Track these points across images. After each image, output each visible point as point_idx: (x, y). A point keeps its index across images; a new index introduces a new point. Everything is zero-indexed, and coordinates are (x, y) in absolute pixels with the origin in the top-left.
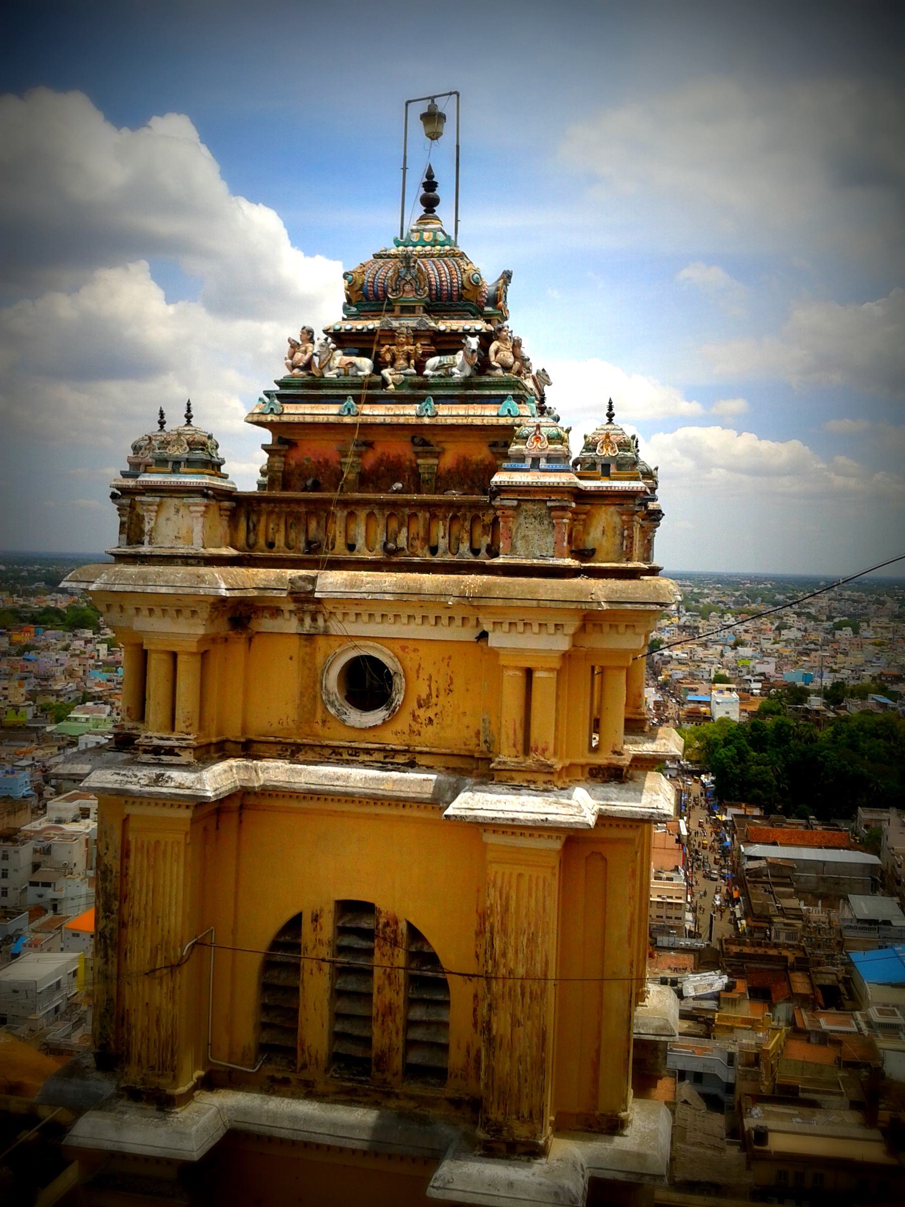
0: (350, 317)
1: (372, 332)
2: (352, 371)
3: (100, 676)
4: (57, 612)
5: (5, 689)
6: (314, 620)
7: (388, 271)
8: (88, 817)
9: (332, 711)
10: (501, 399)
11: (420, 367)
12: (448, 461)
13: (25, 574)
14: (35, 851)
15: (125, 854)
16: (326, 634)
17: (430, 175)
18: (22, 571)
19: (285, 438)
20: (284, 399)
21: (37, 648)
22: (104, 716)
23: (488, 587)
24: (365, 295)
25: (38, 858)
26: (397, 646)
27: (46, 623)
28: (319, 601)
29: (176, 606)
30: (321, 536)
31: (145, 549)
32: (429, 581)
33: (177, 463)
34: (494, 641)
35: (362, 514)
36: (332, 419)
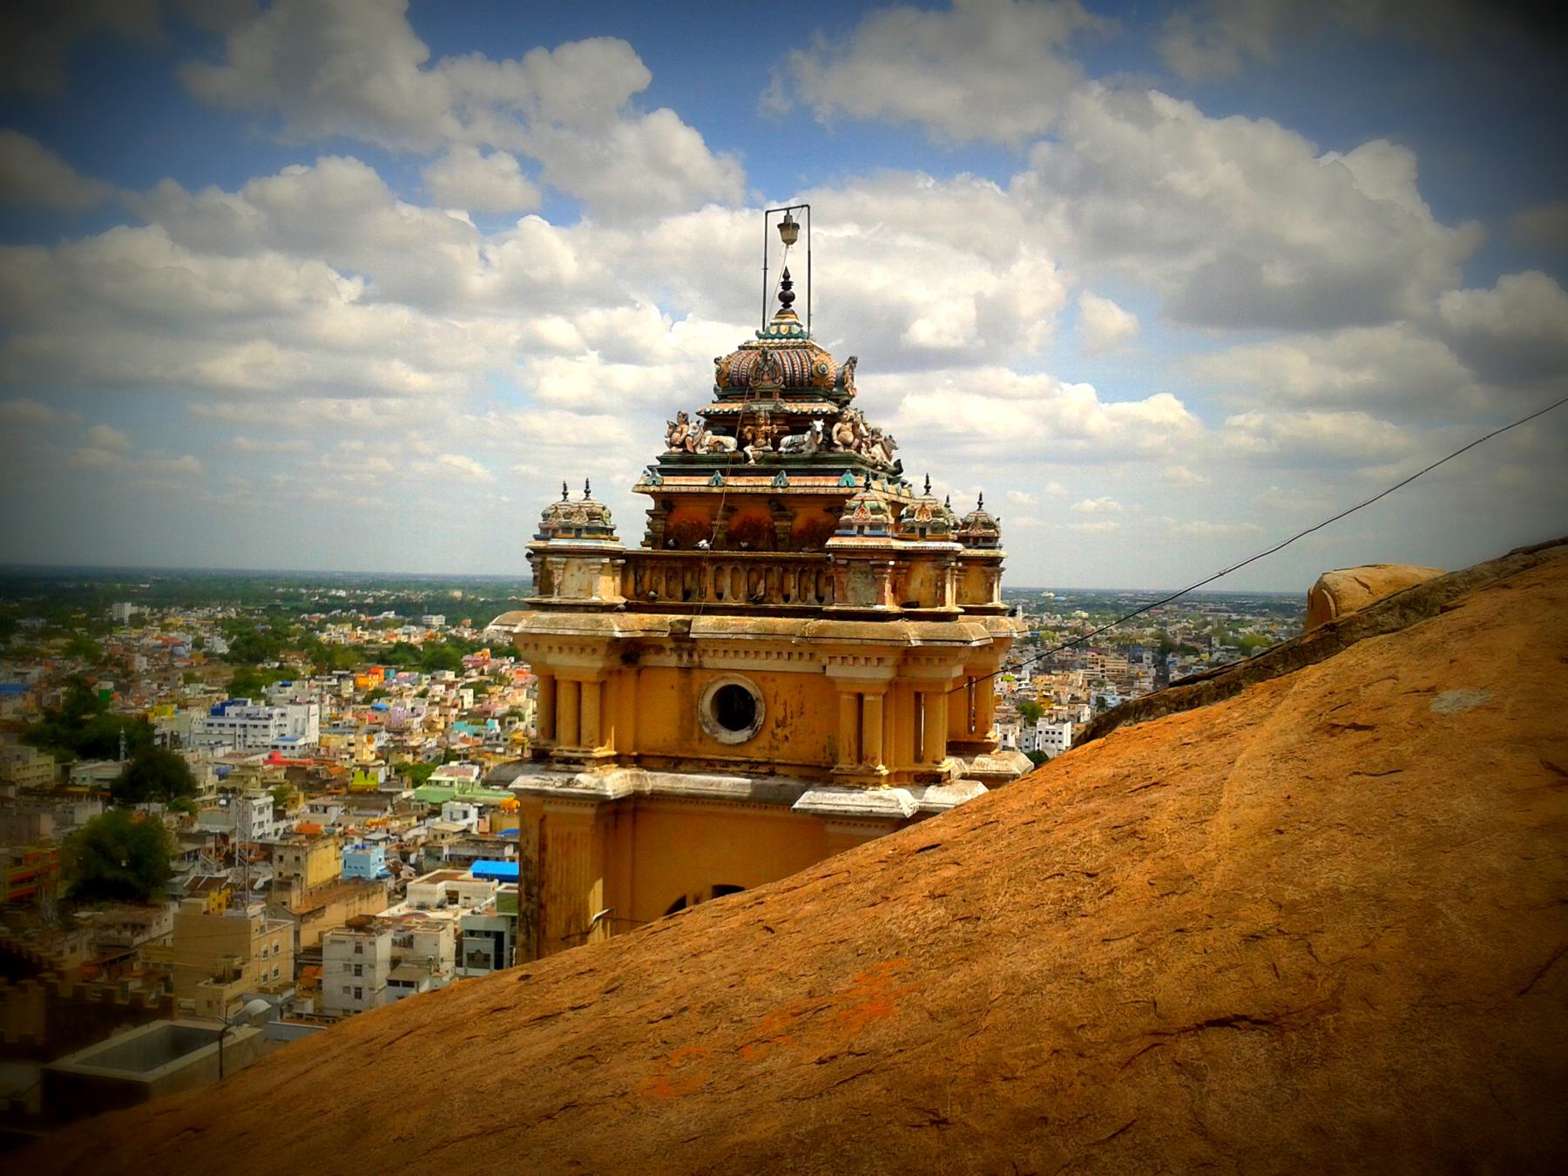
0: (723, 398)
1: (736, 414)
2: (719, 448)
3: (465, 730)
4: (411, 648)
5: (351, 745)
6: (690, 655)
7: (749, 361)
8: (456, 902)
9: (707, 731)
10: (841, 472)
11: (776, 444)
12: (799, 523)
13: (370, 601)
14: (394, 943)
15: (543, 848)
16: (701, 667)
17: (786, 276)
18: (366, 597)
19: (666, 503)
20: (663, 472)
21: (388, 694)
22: (472, 779)
23: (822, 629)
24: (731, 382)
25: (399, 952)
26: (759, 677)
27: (397, 662)
28: (694, 640)
29: (581, 645)
30: (695, 587)
31: (555, 600)
32: (781, 623)
33: (579, 530)
34: (829, 673)
35: (728, 569)
36: (703, 489)
